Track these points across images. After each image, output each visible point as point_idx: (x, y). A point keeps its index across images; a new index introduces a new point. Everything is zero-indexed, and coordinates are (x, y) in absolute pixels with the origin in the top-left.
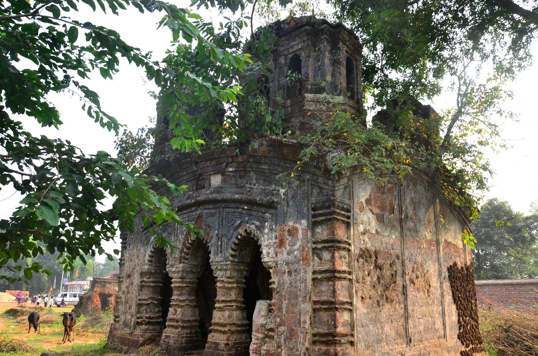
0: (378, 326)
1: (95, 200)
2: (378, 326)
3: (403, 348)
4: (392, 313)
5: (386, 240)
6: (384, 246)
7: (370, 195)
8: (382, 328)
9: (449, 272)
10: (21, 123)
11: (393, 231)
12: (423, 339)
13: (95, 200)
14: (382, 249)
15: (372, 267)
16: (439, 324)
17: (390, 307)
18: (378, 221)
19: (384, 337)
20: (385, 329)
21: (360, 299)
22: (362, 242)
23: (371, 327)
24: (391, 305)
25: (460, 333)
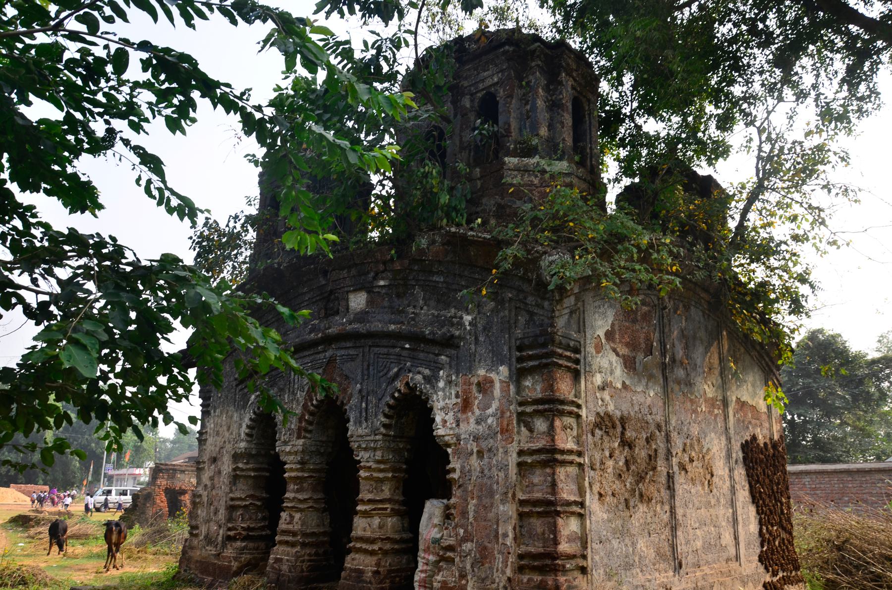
0: (627, 540)
3: (667, 577)
7: (613, 325)
8: (634, 544)
12: (701, 563)
14: (632, 414)
15: (616, 444)
17: (646, 510)
19: (637, 559)
20: (639, 546)
21: (597, 497)
23: (615, 543)
24: (648, 506)
25: (762, 552)
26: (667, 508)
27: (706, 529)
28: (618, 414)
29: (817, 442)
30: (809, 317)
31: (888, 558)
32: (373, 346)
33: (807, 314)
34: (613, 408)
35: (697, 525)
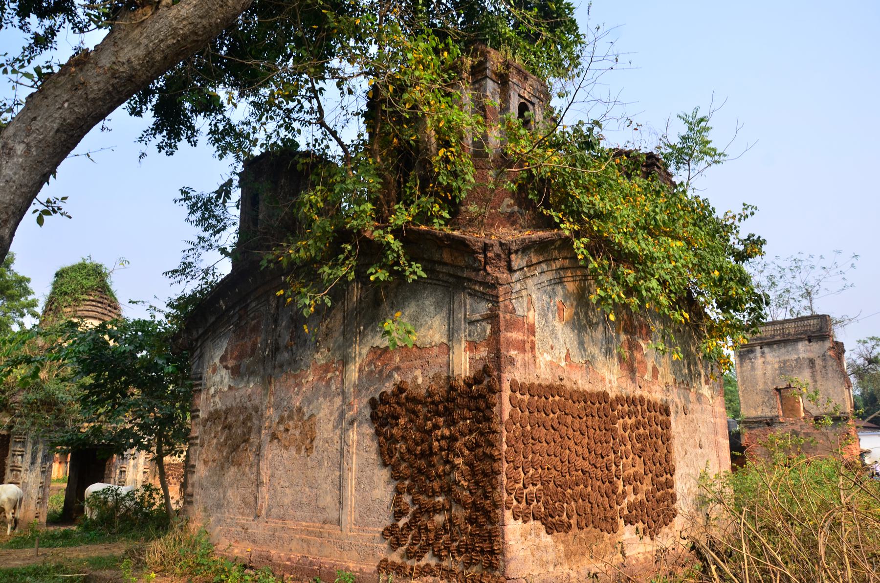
0: (221, 490)
1: (425, 276)
2: (221, 490)
3: (247, 520)
4: (239, 477)
5: (242, 392)
6: (238, 400)
7: (226, 351)
8: (225, 493)
9: (584, 397)
10: (28, 280)
11: (251, 379)
12: (287, 517)
13: (425, 276)
14: (234, 405)
15: (220, 429)
16: (328, 500)
17: (236, 470)
18: (232, 375)
19: (226, 503)
20: (228, 494)
21: (202, 462)
22: (212, 404)
23: (212, 491)
24: (238, 468)
25: (394, 526)
26: (254, 469)
27: (298, 489)
28: (224, 408)
29: (723, 295)
30: (183, 192)
31: (413, 8)
32: (278, 302)
33: (188, 198)
34: (220, 405)
35: (287, 484)
